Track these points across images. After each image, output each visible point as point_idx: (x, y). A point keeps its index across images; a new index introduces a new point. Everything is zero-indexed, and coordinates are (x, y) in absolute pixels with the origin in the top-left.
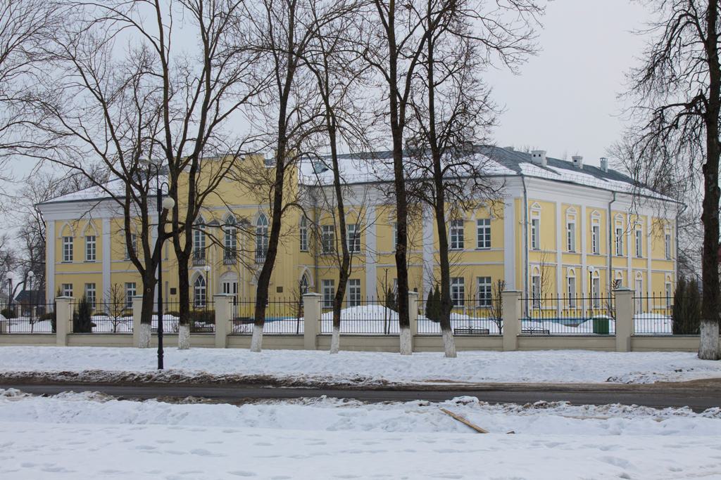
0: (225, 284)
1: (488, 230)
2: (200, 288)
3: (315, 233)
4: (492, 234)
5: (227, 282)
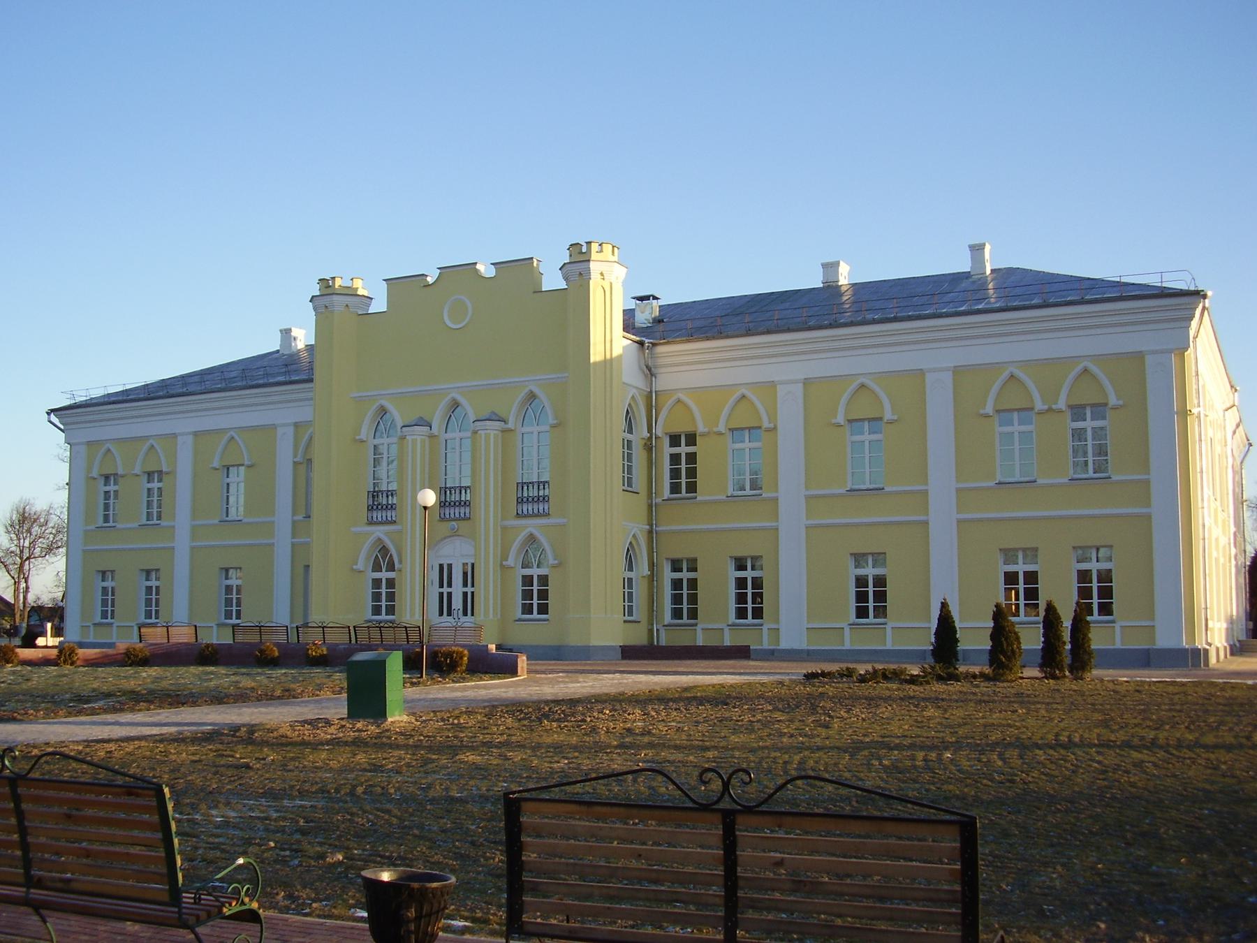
0: (441, 566)
1: (692, 458)
2: (384, 575)
4: (700, 466)
5: (445, 562)
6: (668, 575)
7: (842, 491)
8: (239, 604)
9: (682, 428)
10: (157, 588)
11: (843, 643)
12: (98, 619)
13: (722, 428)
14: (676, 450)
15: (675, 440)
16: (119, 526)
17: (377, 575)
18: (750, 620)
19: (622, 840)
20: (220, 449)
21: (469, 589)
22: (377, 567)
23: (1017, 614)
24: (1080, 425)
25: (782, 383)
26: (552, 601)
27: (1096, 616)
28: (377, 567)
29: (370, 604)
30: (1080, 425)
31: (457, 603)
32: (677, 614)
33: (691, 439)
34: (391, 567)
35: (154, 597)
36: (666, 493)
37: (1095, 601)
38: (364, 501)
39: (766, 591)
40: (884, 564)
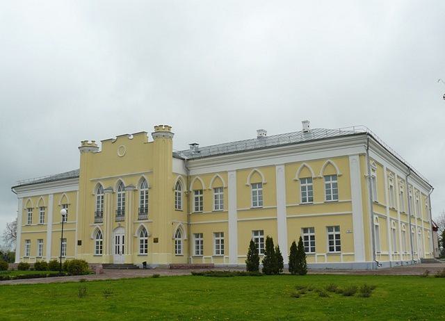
2: (144, 238)
3: (188, 196)
5: (117, 235)
6: (194, 239)
7: (249, 208)
8: (176, 246)
9: (198, 188)
10: (101, 242)
11: (315, 261)
12: (215, 254)
13: (210, 188)
14: (197, 196)
15: (196, 192)
16: (314, 203)
17: (142, 238)
18: (335, 252)
19: (14, 313)
20: (212, 180)
21: (117, 245)
22: (142, 236)
23: (308, 251)
24: (304, 185)
25: (277, 165)
26: (342, 245)
27: (310, 252)
28: (142, 236)
29: (328, 246)
30: (304, 185)
31: (121, 250)
32: (198, 253)
33: (201, 192)
34: (146, 236)
35: (200, 245)
36: (194, 211)
37: (310, 247)
38: (138, 212)
39: (225, 244)
40: (339, 231)
